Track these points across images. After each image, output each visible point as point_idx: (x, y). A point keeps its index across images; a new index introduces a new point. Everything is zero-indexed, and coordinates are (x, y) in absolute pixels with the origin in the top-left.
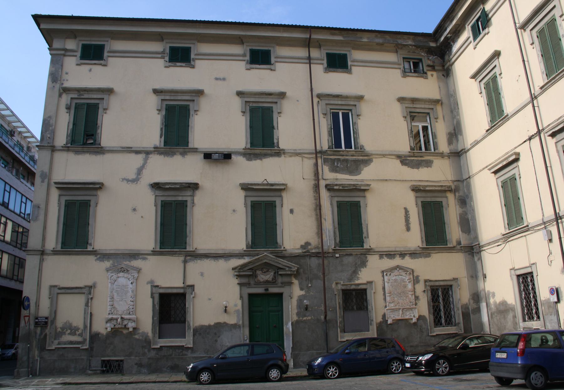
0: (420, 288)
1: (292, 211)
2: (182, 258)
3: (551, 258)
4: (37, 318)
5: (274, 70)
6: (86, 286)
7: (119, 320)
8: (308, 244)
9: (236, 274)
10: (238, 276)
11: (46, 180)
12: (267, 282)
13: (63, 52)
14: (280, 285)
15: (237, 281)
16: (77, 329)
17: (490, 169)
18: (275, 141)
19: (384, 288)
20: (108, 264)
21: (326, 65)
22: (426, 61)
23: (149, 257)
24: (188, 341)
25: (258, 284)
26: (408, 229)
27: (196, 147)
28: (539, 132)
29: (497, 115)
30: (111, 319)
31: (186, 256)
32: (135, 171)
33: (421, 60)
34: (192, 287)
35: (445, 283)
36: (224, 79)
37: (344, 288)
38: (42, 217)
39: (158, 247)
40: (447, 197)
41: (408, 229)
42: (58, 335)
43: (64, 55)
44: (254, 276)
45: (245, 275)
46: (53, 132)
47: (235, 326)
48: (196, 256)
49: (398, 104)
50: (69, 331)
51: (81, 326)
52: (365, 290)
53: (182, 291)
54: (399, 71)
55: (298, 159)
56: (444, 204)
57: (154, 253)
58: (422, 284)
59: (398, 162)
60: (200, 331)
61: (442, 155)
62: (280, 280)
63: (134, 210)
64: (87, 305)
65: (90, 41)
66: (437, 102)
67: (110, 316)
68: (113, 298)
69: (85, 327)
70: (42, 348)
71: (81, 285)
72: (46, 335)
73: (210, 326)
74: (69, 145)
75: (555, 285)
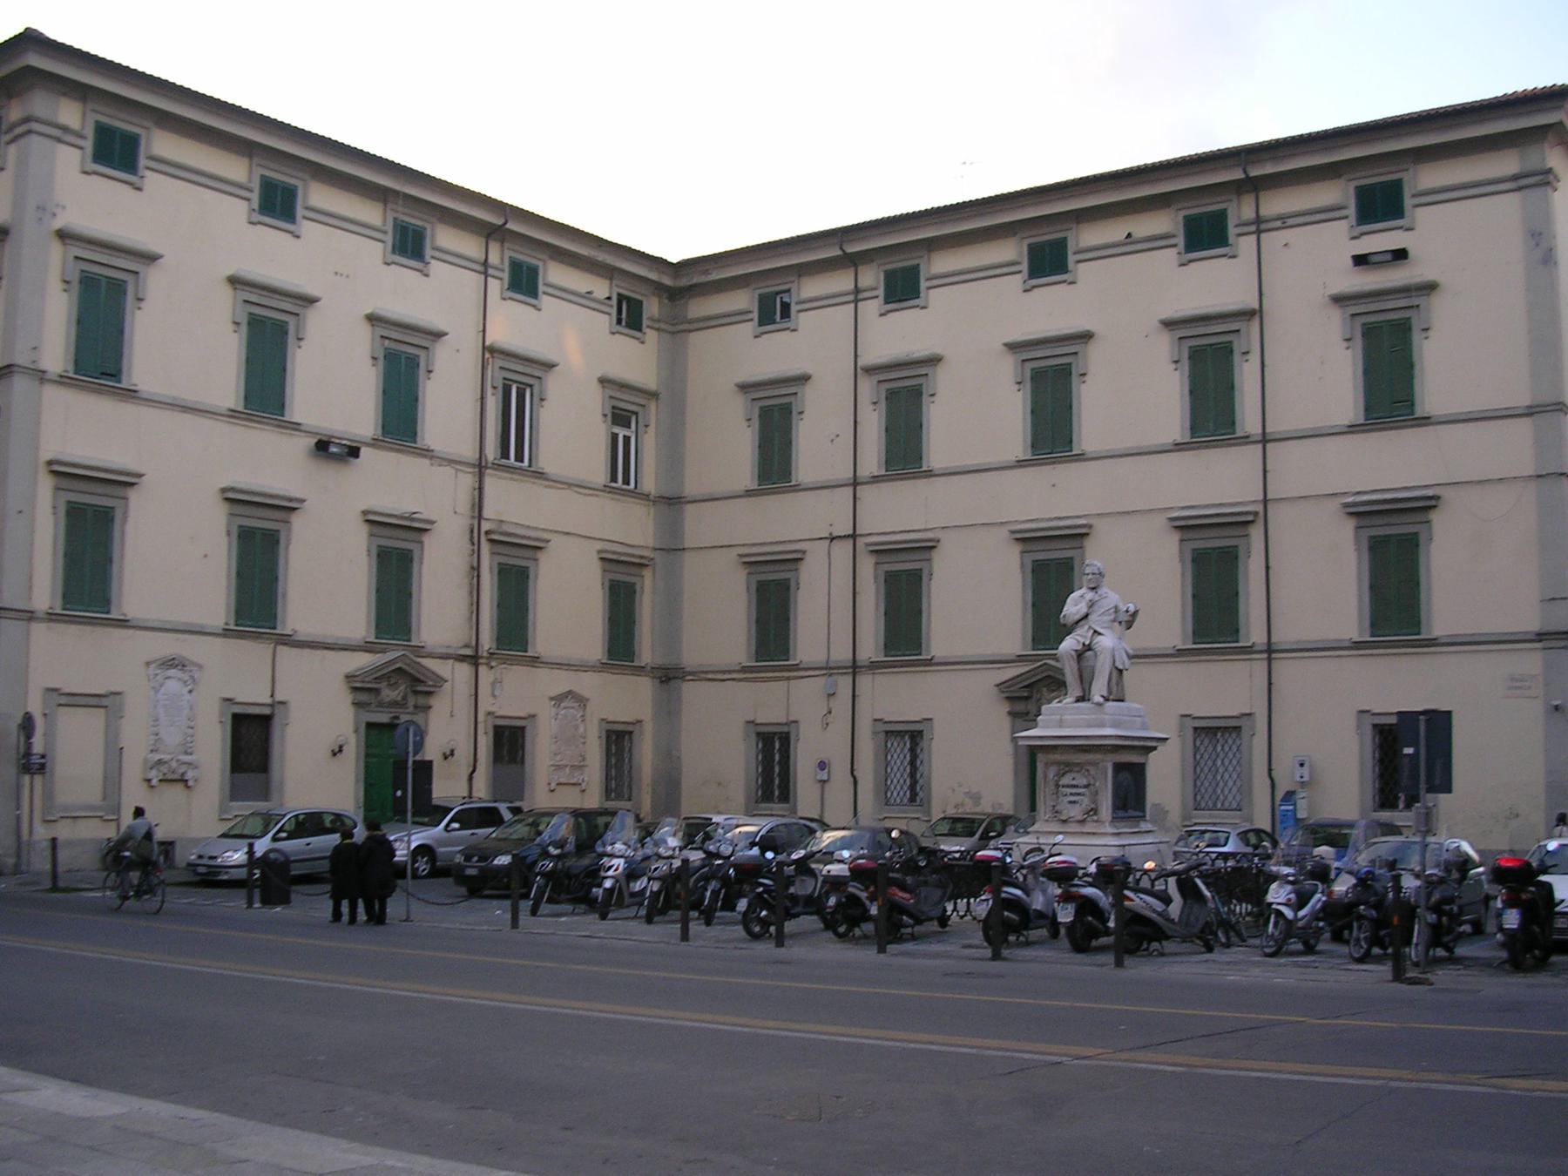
3: (830, 718)
5: (139, 189)
10: (1010, 699)
14: (411, 709)
15: (1006, 707)
21: (256, 205)
28: (854, 536)
30: (160, 762)
35: (621, 727)
39: (232, 622)
40: (421, 543)
43: (59, 140)
45: (363, 689)
49: (226, 293)
52: (523, 729)
53: (267, 711)
55: (448, 471)
56: (638, 588)
57: (227, 633)
62: (411, 701)
66: (654, 395)
67: (157, 757)
75: (823, 756)
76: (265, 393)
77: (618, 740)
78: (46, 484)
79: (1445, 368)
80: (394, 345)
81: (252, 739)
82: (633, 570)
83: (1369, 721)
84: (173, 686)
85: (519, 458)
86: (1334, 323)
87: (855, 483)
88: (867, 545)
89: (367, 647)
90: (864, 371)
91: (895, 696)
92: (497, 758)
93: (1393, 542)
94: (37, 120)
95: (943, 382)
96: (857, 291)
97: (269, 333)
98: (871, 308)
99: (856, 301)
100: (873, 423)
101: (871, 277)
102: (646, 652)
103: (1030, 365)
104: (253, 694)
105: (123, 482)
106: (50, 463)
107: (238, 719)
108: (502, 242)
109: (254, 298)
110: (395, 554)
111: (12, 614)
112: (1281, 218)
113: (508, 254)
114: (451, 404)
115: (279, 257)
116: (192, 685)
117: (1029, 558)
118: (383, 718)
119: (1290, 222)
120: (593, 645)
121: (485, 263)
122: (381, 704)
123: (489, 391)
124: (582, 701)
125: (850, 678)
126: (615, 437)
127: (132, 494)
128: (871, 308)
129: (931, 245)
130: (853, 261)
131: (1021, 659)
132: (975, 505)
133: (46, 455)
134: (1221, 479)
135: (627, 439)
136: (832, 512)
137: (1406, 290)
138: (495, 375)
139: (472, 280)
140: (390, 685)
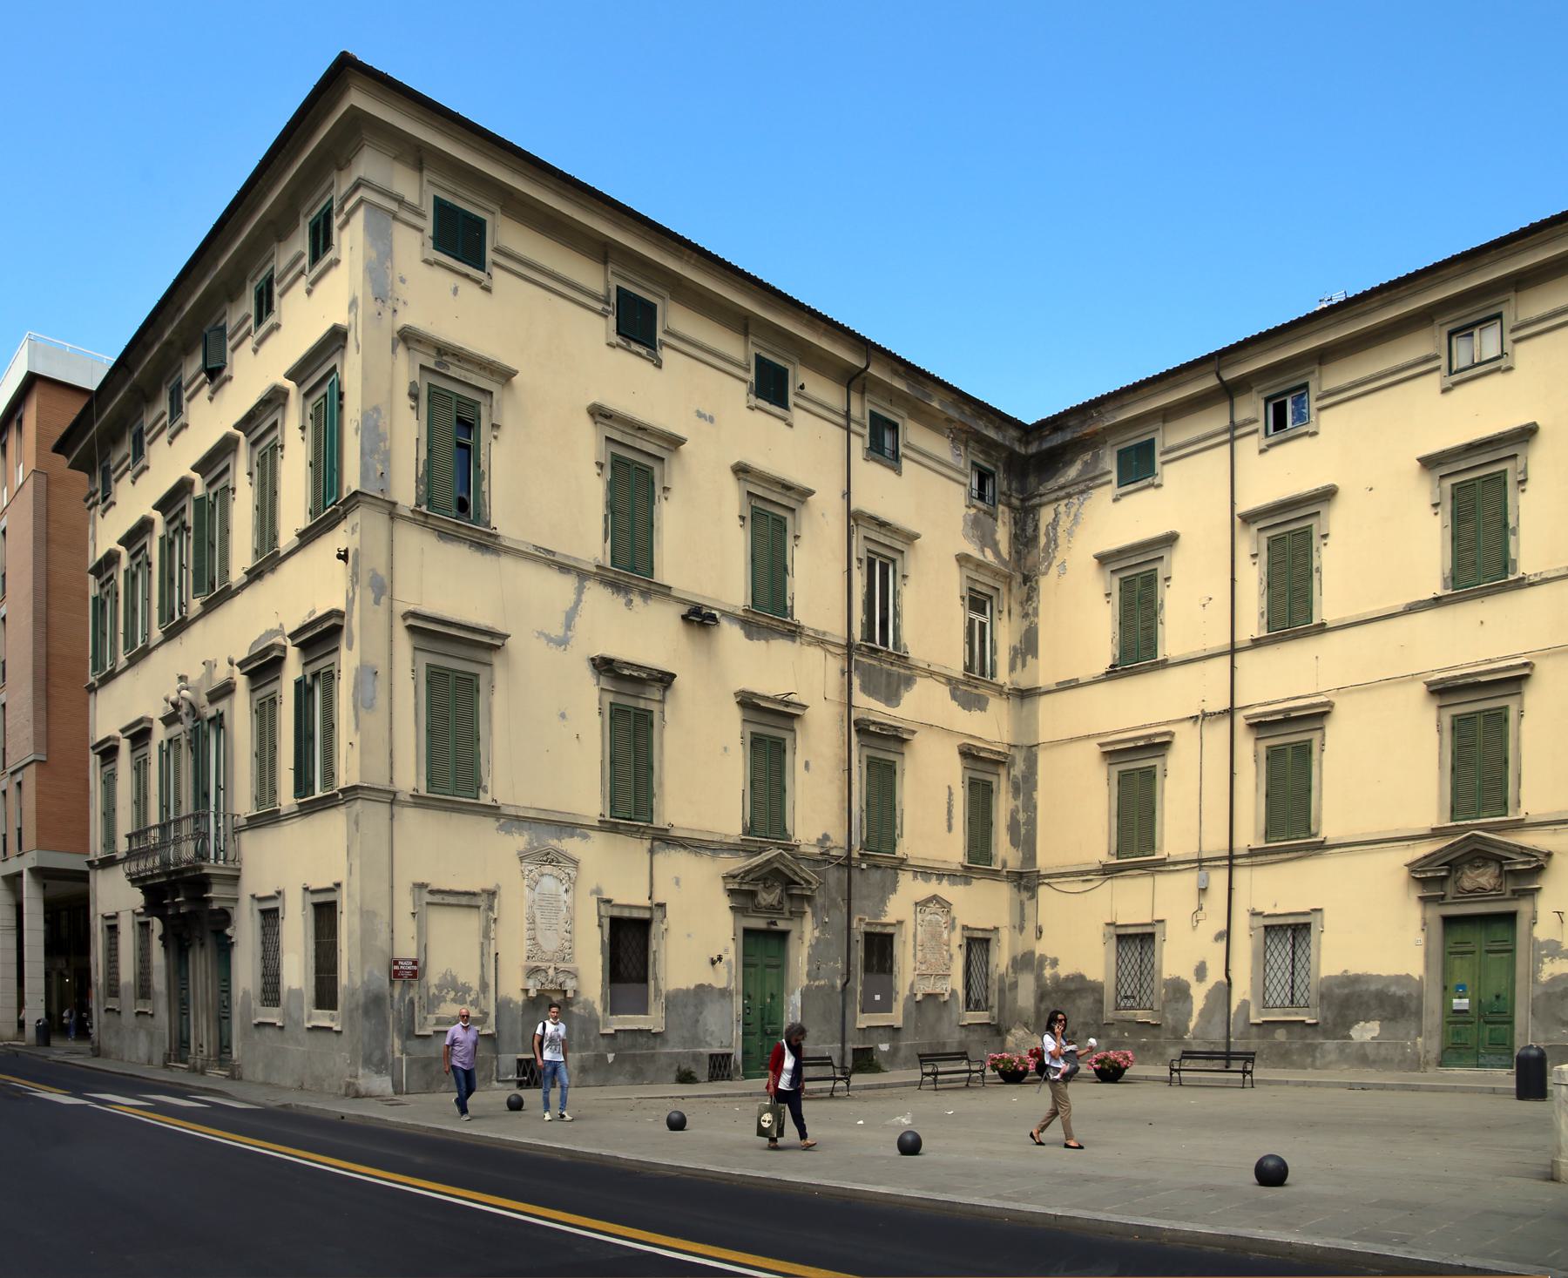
0: (957, 938)
1: (807, 765)
2: (647, 844)
3: (1200, 915)
4: (396, 963)
6: (484, 891)
7: (551, 972)
8: (826, 837)
9: (730, 886)
10: (1424, 882)
11: (384, 599)
12: (771, 908)
13: (393, 206)
14: (787, 915)
15: (1416, 893)
16: (468, 990)
17: (1101, 745)
18: (789, 603)
19: (915, 936)
20: (519, 841)
22: (1001, 481)
23: (592, 833)
24: (653, 1020)
25: (758, 910)
26: (950, 828)
27: (395, 499)
28: (1231, 712)
29: (1137, 651)
31: (654, 839)
32: (561, 618)
33: (992, 475)
34: (662, 906)
36: (711, 420)
37: (869, 929)
38: (382, 700)
40: (793, 730)
41: (950, 828)
42: (433, 1003)
43: (395, 217)
44: (752, 894)
45: (742, 895)
46: (387, 458)
47: (724, 993)
48: (665, 839)
50: (452, 994)
51: (475, 984)
52: (891, 936)
53: (647, 915)
54: (961, 489)
58: (958, 929)
59: (944, 691)
60: (674, 1001)
61: (999, 690)
62: (787, 906)
63: (563, 716)
64: (486, 934)
65: (455, 195)
68: (534, 922)
69: (484, 986)
70: (409, 1034)
71: (476, 889)
72: (412, 1002)
73: (688, 990)
74: (424, 508)
76: (631, 563)
77: (978, 944)
78: (404, 644)
80: (760, 504)
81: (629, 941)
82: (991, 768)
84: (549, 884)
85: (884, 641)
87: (1233, 651)
88: (1247, 718)
91: (1277, 889)
95: (1337, 520)
96: (1234, 426)
97: (635, 473)
99: (1232, 441)
100: (1252, 578)
101: (1252, 408)
102: (1004, 850)
103: (1448, 483)
104: (631, 895)
107: (616, 923)
108: (863, 393)
109: (617, 436)
111: (373, 795)
113: (869, 407)
116: (572, 884)
117: (1447, 715)
118: (759, 923)
120: (954, 851)
121: (847, 415)
123: (855, 563)
124: (945, 905)
125: (1224, 873)
126: (971, 621)
128: (1248, 447)
129: (1324, 356)
130: (1229, 392)
131: (1436, 833)
133: (400, 608)
135: (983, 625)
136: (1205, 687)
139: (836, 435)
140: (766, 888)
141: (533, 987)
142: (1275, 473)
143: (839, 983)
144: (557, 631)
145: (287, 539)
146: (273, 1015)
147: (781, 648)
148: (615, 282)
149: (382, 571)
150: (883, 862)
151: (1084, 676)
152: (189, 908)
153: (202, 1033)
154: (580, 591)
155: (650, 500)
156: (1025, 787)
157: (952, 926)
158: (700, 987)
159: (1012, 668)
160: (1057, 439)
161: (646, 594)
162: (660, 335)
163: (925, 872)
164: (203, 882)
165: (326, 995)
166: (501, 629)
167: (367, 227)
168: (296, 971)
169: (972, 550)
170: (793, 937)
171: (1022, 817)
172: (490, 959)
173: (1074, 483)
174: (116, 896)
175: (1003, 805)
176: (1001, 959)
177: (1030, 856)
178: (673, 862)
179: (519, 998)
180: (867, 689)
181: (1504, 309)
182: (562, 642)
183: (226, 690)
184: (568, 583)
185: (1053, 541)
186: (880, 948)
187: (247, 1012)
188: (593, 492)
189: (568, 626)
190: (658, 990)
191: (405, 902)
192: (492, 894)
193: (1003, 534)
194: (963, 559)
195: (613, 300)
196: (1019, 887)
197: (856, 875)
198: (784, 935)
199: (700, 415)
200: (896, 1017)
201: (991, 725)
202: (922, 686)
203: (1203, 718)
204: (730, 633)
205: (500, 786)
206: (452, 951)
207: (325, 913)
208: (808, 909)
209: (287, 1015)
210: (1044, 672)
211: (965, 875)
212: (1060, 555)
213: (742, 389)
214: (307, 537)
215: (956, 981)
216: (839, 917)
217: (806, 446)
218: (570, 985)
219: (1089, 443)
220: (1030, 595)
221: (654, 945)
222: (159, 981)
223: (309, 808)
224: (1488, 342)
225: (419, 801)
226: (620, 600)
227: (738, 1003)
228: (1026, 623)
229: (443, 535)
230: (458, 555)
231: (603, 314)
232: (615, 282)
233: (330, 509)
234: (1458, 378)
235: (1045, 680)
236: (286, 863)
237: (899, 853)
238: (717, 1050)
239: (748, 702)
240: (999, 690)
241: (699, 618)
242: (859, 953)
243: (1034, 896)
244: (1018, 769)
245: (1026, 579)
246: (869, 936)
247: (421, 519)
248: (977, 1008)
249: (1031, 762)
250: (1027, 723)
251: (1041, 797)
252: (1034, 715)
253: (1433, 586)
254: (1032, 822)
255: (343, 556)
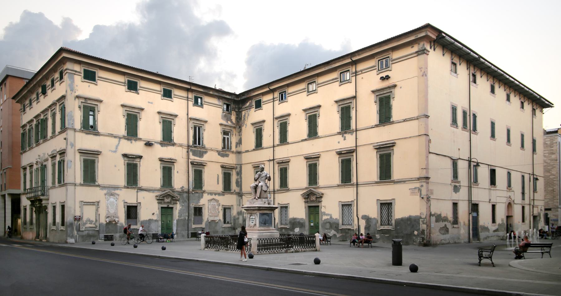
0: (220, 208)
2: (136, 190)
8: (183, 187)
12: (168, 202)
13: (74, 72)
15: (304, 200)
20: (105, 191)
22: (232, 106)
26: (218, 183)
28: (273, 160)
34: (140, 203)
41: (218, 183)
44: (163, 200)
45: (160, 200)
47: (156, 221)
48: (141, 189)
51: (94, 220)
57: (125, 187)
69: (96, 221)
70: (79, 230)
76: (132, 131)
77: (226, 210)
78: (78, 155)
79: (400, 108)
81: (132, 211)
83: (341, 203)
85: (199, 144)
86: (373, 97)
89: (158, 190)
90: (275, 118)
92: (195, 214)
93: (385, 154)
94: (68, 69)
96: (274, 98)
98: (277, 102)
100: (277, 131)
103: (308, 115)
104: (132, 201)
105: (97, 153)
106: (78, 150)
110: (167, 168)
112: (361, 71)
113: (194, 95)
114: (181, 133)
115: (134, 99)
118: (165, 206)
119: (363, 72)
121: (188, 97)
122: (165, 203)
124: (217, 201)
126: (224, 138)
127: (100, 157)
128: (277, 102)
129: (288, 85)
132: (296, 151)
133: (77, 148)
134: (348, 142)
135: (228, 138)
137: (389, 87)
138: (191, 125)
141: (108, 220)
142: (281, 109)
143: (187, 218)
144: (114, 150)
145: (57, 133)
146: (54, 228)
147: (170, 148)
148: (127, 79)
149: (73, 142)
150: (199, 192)
151: (250, 149)
152: (39, 206)
153: (42, 233)
154: (119, 141)
155: (137, 121)
156: (239, 173)
157: (219, 205)
158: (150, 220)
159: (236, 147)
160: (244, 97)
161: (135, 140)
162: (138, 88)
163: (211, 194)
164: (41, 200)
165: (63, 224)
166: (100, 151)
167: (69, 77)
168: (58, 219)
169: (224, 122)
170: (174, 209)
171: (239, 180)
172: (98, 215)
173: (247, 107)
174: (25, 202)
175: (234, 178)
176: (234, 212)
177: (241, 189)
178: (142, 194)
179: (105, 223)
180: (194, 154)
181: (316, 80)
182: (115, 152)
183: (47, 160)
184: (116, 140)
185: (244, 119)
186: (198, 211)
187: (50, 228)
188: (122, 122)
189: (117, 148)
190: (139, 221)
191: (78, 205)
192: (98, 202)
193: (233, 118)
194: (221, 125)
195: (127, 82)
196: (239, 196)
197: (191, 195)
198: (172, 208)
199: (149, 102)
200: (203, 226)
201: (231, 160)
202: (209, 153)
203: (270, 160)
204: (157, 147)
205: (100, 180)
206: (89, 214)
207: (63, 207)
208: (178, 202)
209: (57, 228)
210: (243, 148)
211: (223, 194)
212: (246, 122)
213: (160, 95)
214: (60, 133)
215: (221, 217)
216: (186, 204)
217: (178, 105)
218: (117, 220)
219: (250, 98)
220: (240, 131)
221: (138, 211)
222: (34, 221)
223: (60, 186)
224: (312, 87)
225: (81, 185)
226: (129, 142)
227: (160, 223)
228: (239, 137)
229: (87, 134)
230: (91, 137)
231: (124, 86)
232: (127, 79)
233: (64, 129)
234: (309, 93)
235: (243, 150)
236: (55, 196)
237: (203, 189)
238: (154, 233)
239: (161, 160)
240: (233, 152)
241: (149, 144)
242: (192, 212)
243: (242, 198)
244: (238, 170)
245: (240, 127)
246: (195, 209)
247: (81, 131)
248: (228, 223)
249: (241, 168)
250: (239, 159)
251: (243, 176)
252: (241, 158)
253: (254, 148)
254: (241, 181)
255: (65, 139)
